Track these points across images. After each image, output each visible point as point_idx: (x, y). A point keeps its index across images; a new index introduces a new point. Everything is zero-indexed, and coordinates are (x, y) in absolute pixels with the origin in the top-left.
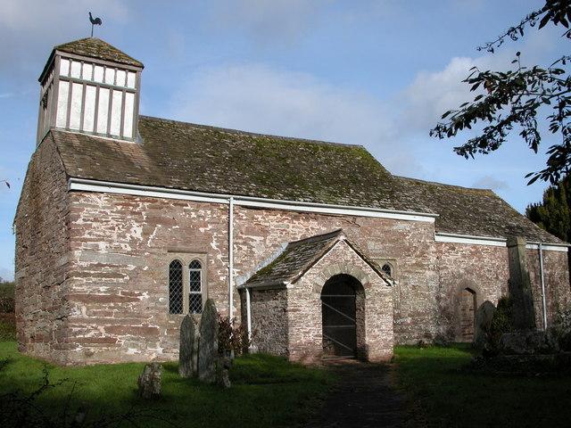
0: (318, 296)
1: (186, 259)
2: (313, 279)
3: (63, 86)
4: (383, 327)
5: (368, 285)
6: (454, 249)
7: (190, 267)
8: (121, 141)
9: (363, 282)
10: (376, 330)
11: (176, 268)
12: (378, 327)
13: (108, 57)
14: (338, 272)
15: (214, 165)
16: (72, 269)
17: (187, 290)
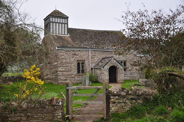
0: (108, 70)
1: (81, 62)
2: (107, 67)
3: (51, 24)
4: (122, 76)
5: (119, 68)
8: (61, 35)
9: (118, 67)
11: (79, 64)
13: (61, 16)
14: (112, 65)
15: (85, 40)
17: (81, 68)
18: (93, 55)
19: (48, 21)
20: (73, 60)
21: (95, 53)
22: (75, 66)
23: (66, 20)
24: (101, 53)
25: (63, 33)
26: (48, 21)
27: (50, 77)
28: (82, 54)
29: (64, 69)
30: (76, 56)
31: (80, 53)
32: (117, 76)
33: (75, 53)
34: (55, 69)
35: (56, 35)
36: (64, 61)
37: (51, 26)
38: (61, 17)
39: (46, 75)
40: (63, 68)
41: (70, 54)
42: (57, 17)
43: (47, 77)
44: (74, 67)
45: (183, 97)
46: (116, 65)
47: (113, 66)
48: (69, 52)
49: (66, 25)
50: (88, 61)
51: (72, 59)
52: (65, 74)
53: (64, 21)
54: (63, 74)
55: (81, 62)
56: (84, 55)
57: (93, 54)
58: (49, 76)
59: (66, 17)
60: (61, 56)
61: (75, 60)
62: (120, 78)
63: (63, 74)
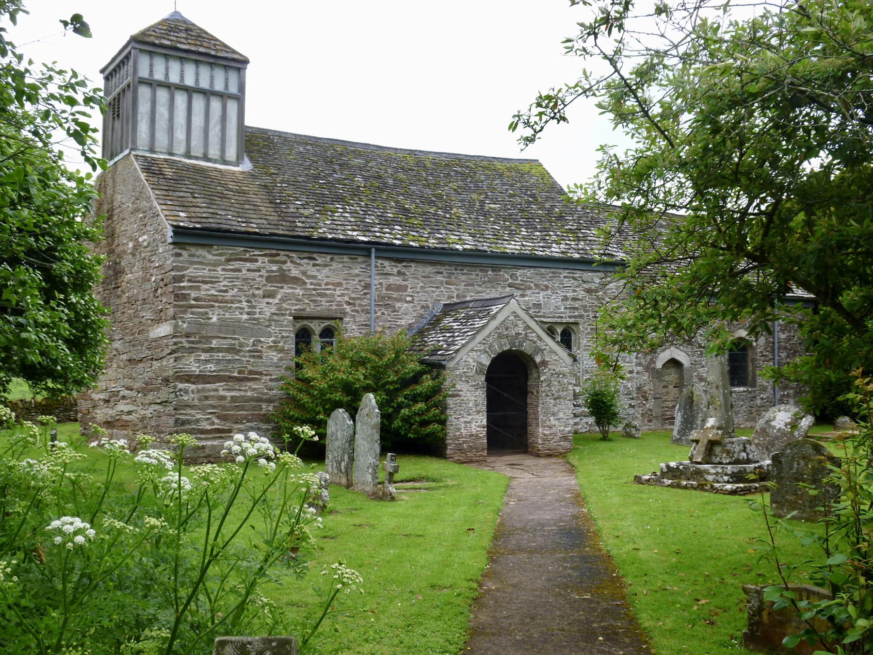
1: (317, 327)
3: (144, 92)
4: (561, 415)
5: (544, 363)
6: (732, 406)
7: (321, 336)
9: (538, 359)
10: (552, 418)
12: (553, 415)
16: (71, 334)
18: (389, 288)
19: (124, 78)
20: (268, 311)
21: (399, 273)
22: (282, 350)
23: (233, 77)
24: (439, 278)
25: (214, 152)
26: (124, 78)
27: (129, 413)
28: (326, 280)
29: (211, 367)
30: (286, 290)
31: (312, 271)
32: (530, 411)
33: (280, 269)
34: (156, 364)
35: (166, 160)
36: (215, 319)
37: (144, 108)
38: (201, 54)
39: (107, 401)
40: (207, 361)
41: (251, 275)
42: (212, 60)
43: (111, 412)
44: (275, 356)
45: (871, 36)
46: (526, 348)
47: (510, 351)
48: (248, 264)
49: (232, 106)
50: (362, 318)
51: (266, 309)
52: (222, 393)
53: (219, 80)
54: (206, 398)
55: (317, 327)
56: (339, 284)
57: (392, 280)
58: (123, 407)
59: (236, 56)
60: (198, 288)
61: (280, 312)
62: (550, 427)
63: (206, 398)
